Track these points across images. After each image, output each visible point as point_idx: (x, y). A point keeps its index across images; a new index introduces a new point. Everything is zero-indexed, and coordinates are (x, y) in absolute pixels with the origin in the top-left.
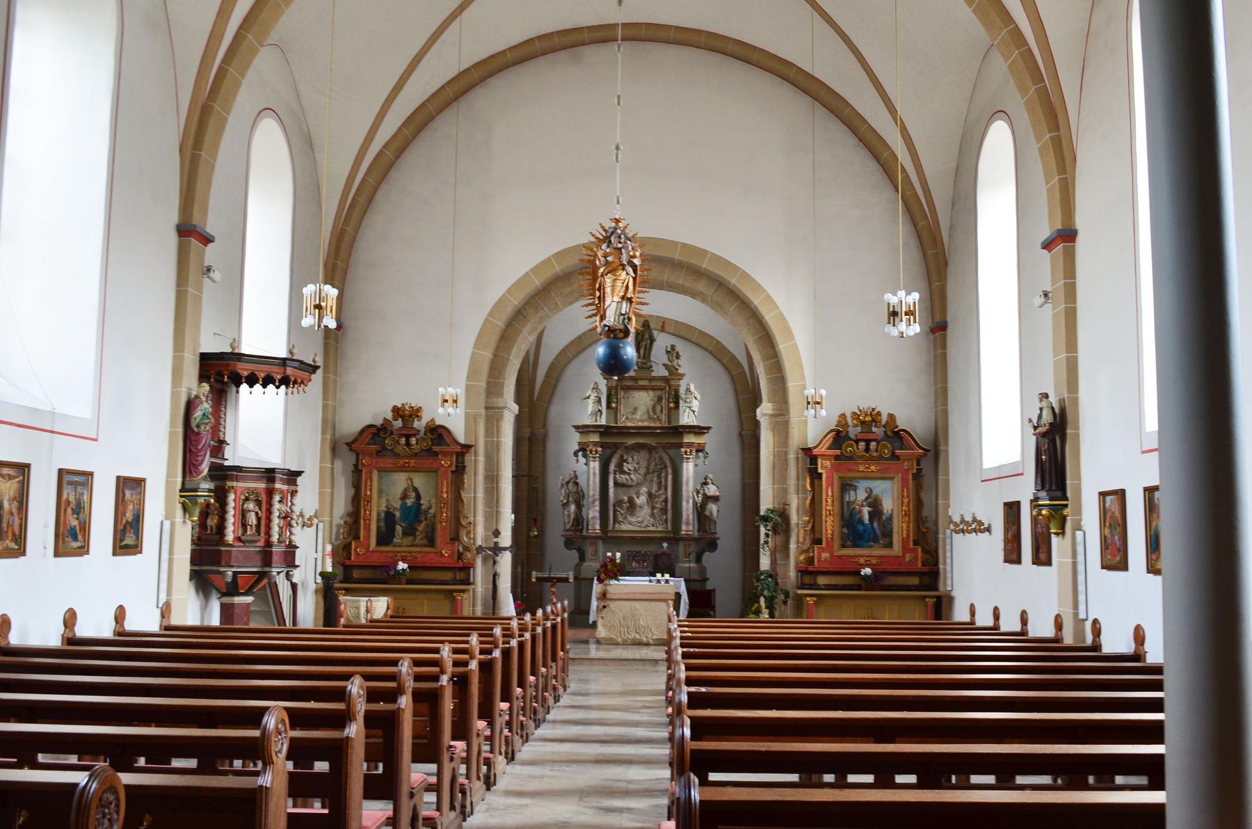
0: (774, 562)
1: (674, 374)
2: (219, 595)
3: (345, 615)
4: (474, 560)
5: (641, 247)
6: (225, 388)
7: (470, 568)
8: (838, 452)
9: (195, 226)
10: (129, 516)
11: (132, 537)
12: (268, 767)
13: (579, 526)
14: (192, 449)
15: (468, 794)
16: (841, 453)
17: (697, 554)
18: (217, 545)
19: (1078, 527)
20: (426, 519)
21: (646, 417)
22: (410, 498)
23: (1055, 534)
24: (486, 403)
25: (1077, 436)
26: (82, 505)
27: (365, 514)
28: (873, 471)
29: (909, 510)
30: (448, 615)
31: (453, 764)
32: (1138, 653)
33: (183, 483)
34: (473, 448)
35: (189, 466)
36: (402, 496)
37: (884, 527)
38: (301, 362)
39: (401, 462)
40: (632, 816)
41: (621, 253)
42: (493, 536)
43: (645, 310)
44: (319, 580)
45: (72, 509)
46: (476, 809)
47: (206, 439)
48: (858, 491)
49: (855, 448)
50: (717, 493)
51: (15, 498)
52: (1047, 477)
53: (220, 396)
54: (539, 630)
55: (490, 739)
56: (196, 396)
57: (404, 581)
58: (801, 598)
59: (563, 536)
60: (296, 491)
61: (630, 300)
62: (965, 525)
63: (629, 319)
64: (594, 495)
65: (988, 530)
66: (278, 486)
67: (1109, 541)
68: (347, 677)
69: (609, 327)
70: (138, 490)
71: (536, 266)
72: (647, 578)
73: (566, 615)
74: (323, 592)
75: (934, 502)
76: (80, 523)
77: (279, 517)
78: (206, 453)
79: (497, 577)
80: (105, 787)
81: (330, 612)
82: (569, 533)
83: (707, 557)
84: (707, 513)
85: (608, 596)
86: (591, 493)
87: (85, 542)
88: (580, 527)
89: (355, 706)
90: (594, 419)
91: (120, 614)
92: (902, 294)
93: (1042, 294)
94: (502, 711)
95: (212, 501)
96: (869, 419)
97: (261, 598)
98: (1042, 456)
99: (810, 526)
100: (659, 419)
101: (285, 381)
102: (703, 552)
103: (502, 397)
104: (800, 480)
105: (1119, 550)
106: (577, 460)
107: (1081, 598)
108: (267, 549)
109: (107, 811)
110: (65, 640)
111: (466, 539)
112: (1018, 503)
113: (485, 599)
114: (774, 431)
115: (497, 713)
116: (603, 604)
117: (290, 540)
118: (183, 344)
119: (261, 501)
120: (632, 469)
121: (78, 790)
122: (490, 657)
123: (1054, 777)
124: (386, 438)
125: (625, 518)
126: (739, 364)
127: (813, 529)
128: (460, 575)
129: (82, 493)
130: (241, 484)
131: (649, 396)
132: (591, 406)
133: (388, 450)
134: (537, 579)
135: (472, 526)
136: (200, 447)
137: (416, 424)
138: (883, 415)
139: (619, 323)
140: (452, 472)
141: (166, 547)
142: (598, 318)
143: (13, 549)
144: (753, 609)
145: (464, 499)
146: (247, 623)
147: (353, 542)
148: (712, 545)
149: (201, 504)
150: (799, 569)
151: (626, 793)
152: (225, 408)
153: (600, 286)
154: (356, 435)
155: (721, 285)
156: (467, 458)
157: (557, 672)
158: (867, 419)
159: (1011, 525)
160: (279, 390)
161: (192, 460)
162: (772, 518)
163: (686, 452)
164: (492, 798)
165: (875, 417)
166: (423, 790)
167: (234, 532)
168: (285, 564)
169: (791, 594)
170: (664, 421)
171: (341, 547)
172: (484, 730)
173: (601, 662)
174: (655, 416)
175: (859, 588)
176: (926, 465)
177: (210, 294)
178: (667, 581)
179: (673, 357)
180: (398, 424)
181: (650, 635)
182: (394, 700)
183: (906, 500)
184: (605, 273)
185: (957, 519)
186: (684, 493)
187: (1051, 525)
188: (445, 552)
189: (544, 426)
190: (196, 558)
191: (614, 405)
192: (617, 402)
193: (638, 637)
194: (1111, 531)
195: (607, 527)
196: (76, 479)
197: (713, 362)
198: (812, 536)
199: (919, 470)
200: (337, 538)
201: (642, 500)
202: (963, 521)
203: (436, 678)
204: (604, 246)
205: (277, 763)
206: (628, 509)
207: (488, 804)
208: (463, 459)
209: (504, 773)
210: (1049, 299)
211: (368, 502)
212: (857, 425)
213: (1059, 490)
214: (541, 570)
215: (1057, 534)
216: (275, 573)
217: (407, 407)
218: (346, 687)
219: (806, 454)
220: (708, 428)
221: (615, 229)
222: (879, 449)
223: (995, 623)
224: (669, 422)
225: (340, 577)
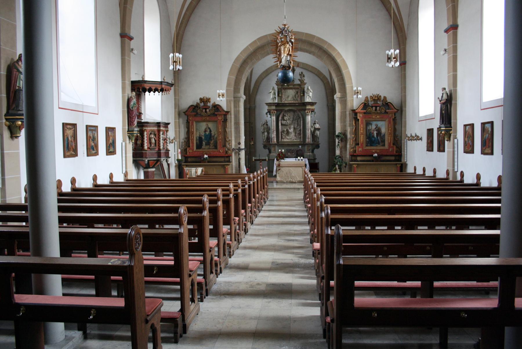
0: (341, 152)
1: (302, 83)
2: (143, 168)
4: (231, 154)
5: (294, 35)
6: (140, 93)
7: (230, 156)
8: (365, 111)
9: (127, 34)
10: (111, 141)
14: (131, 116)
16: (366, 111)
18: (141, 150)
19: (455, 138)
21: (292, 99)
23: (446, 140)
24: (234, 95)
25: (456, 104)
27: (191, 138)
28: (378, 118)
29: (391, 132)
30: (223, 173)
32: (478, 183)
34: (230, 113)
35: (130, 122)
37: (382, 138)
38: (167, 83)
39: (204, 118)
40: (298, 243)
41: (287, 37)
42: (238, 145)
43: (296, 59)
44: (176, 162)
46: (243, 241)
47: (135, 113)
48: (372, 125)
49: (371, 109)
50: (319, 127)
51: (72, 136)
52: (445, 119)
54: (259, 178)
55: (245, 216)
57: (207, 162)
58: (351, 165)
59: (263, 144)
60: (168, 130)
61: (290, 55)
62: (412, 137)
63: (291, 62)
64: (274, 129)
65: (421, 139)
66: (162, 128)
67: (467, 143)
68: (202, 195)
69: (283, 66)
70: (113, 132)
72: (295, 159)
73: (267, 172)
74: (178, 166)
75: (400, 129)
76: (95, 144)
77: (162, 140)
78: (136, 118)
79: (240, 159)
80: (136, 233)
81: (181, 173)
82: (265, 143)
83: (316, 151)
84: (316, 134)
85: (280, 165)
86: (273, 128)
88: (269, 141)
89: (206, 205)
90: (273, 101)
91: (111, 176)
92: (392, 51)
93: (444, 50)
94: (249, 206)
95: (139, 135)
96: (376, 99)
97: (157, 169)
98: (442, 111)
99: (355, 139)
100: (298, 101)
101: (162, 90)
102: (314, 149)
104: (351, 121)
105: (471, 146)
106: (267, 116)
107: (456, 164)
109: (137, 241)
110: (94, 185)
111: (228, 146)
112: (433, 129)
113: (236, 168)
114: (341, 104)
115: (247, 207)
116: (278, 168)
118: (125, 78)
122: (244, 188)
123: (446, 227)
124: (198, 110)
125: (285, 137)
126: (327, 79)
127: (356, 140)
128: (227, 159)
129: (95, 134)
131: (293, 91)
132: (272, 96)
134: (255, 160)
136: (133, 115)
137: (208, 104)
139: (286, 64)
140: (223, 121)
141: (124, 152)
142: (279, 62)
143: (73, 154)
144: (334, 169)
146: (153, 178)
147: (188, 148)
148: (318, 146)
149: (135, 136)
150: (350, 154)
151: (294, 235)
152: (141, 101)
153: (279, 50)
155: (320, 48)
156: (228, 116)
157: (265, 193)
158: (376, 98)
159: (429, 137)
161: (131, 120)
162: (340, 136)
163: (307, 112)
164: (247, 237)
166: (226, 234)
167: (147, 145)
168: (166, 156)
169: (348, 163)
170: (299, 101)
171: (184, 149)
173: (279, 189)
174: (296, 99)
175: (373, 161)
176: (398, 115)
177: (133, 58)
178: (302, 160)
179: (302, 76)
180: (202, 104)
181: (296, 179)
182: (216, 203)
183: (390, 129)
184: (281, 44)
185: (409, 135)
186: (307, 127)
187: (445, 137)
188: (221, 151)
189: (254, 104)
190: (135, 155)
191: (280, 95)
192: (281, 94)
193: (292, 180)
195: (279, 140)
197: (317, 78)
198: (355, 142)
201: (291, 130)
202: (411, 136)
204: (280, 35)
206: (286, 134)
208: (226, 116)
209: (250, 228)
210: (446, 52)
211: (192, 133)
212: (372, 101)
213: (449, 124)
214: (255, 157)
215: (447, 140)
216: (162, 160)
217: (205, 98)
218: (202, 199)
219: (353, 112)
220: (316, 103)
221: (284, 28)
222: (380, 110)
224: (301, 101)
225: (184, 161)
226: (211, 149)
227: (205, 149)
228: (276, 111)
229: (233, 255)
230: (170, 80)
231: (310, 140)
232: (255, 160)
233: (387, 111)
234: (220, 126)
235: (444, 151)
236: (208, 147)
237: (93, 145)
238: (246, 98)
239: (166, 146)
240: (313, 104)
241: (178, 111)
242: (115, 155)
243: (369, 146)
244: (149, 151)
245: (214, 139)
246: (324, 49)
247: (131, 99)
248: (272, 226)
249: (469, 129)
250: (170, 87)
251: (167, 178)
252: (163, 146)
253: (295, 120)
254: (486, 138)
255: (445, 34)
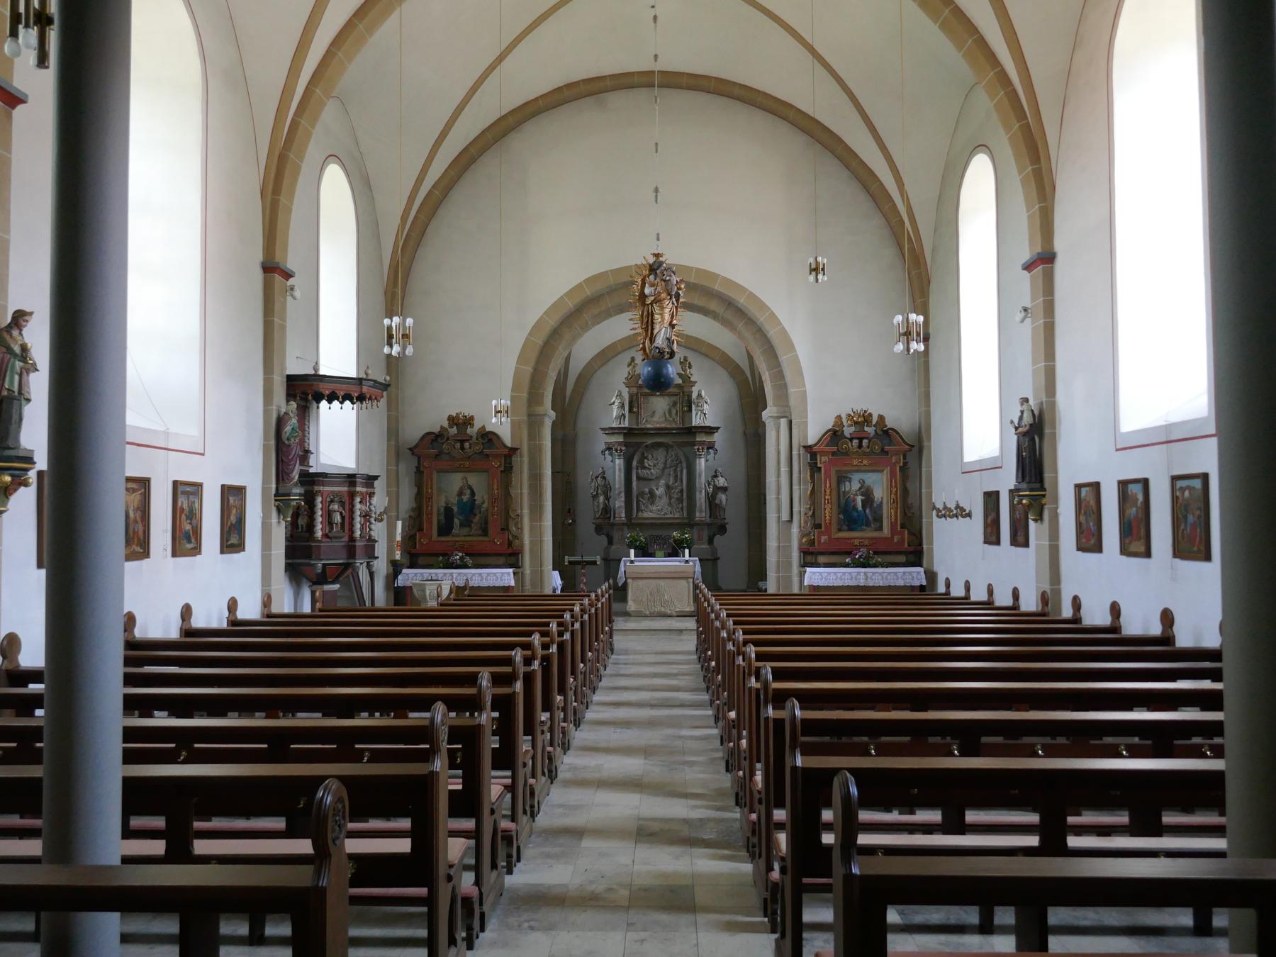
1: (686, 379)
6: (308, 405)
7: (518, 554)
9: (278, 263)
10: (233, 519)
11: (236, 537)
13: (607, 514)
14: (284, 458)
17: (709, 537)
18: (307, 541)
21: (663, 419)
23: (1033, 520)
25: (1054, 435)
26: (194, 511)
29: (897, 498)
33: (277, 489)
34: (519, 451)
35: (282, 475)
38: (375, 381)
39: (457, 464)
45: (186, 515)
47: (296, 451)
49: (850, 445)
51: (138, 508)
53: (304, 412)
55: (564, 709)
56: (285, 413)
59: (593, 523)
60: (374, 493)
64: (619, 488)
65: (969, 515)
66: (359, 489)
67: (1084, 526)
70: (240, 497)
71: (570, 291)
73: (611, 591)
76: (192, 527)
77: (360, 516)
82: (600, 521)
83: (718, 539)
86: (617, 486)
87: (197, 543)
88: (609, 515)
93: (1021, 309)
95: (303, 503)
97: (346, 585)
98: (1022, 453)
100: (676, 423)
101: (361, 398)
108: (350, 544)
112: (998, 493)
117: (370, 535)
119: (344, 503)
120: (652, 464)
121: (316, 800)
125: (647, 507)
126: (743, 372)
129: (194, 502)
130: (326, 488)
132: (615, 412)
134: (569, 562)
136: (290, 457)
137: (469, 430)
138: (873, 416)
140: (501, 471)
145: (513, 495)
148: (722, 529)
149: (294, 506)
152: (309, 422)
154: (417, 442)
163: (698, 449)
165: (866, 418)
167: (322, 529)
174: (671, 419)
180: (454, 430)
183: (894, 490)
185: (940, 506)
186: (697, 485)
190: (291, 552)
194: (1086, 519)
195: (632, 515)
196: (188, 489)
199: (905, 464)
201: (660, 491)
202: (945, 508)
206: (649, 499)
210: (1028, 313)
211: (429, 499)
220: (719, 428)
223: (989, 598)
227: (458, 536)
228: (625, 446)
230: (382, 377)
231: (704, 514)
233: (887, 448)
234: (495, 481)
235: (1026, 544)
236: (466, 530)
237: (189, 530)
238: (556, 416)
239: (368, 530)
240: (712, 431)
242: (242, 553)
243: (844, 530)
244: (328, 542)
245: (480, 513)
246: (739, 306)
247: (286, 417)
249: (1088, 496)
251: (368, 604)
253: (670, 468)
254: (1132, 516)
255: (1026, 272)
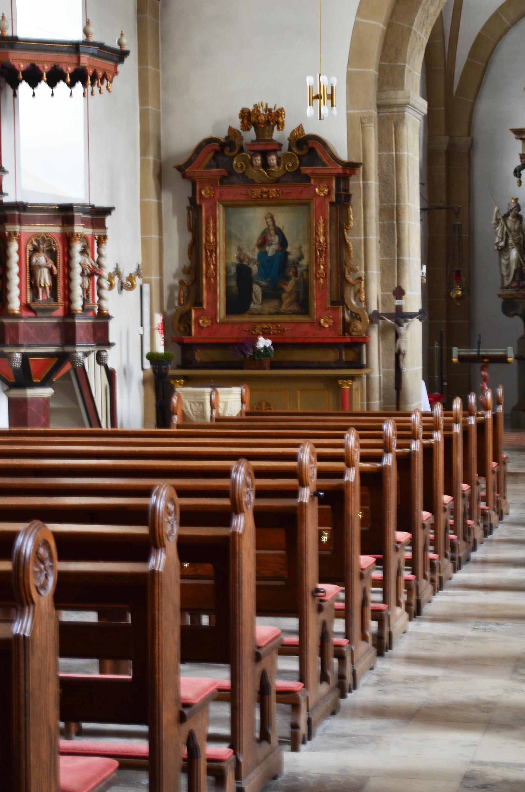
2: (6, 387)
3: (179, 412)
4: (367, 333)
12: (27, 610)
15: (348, 659)
20: (296, 275)
22: (272, 244)
24: (378, 99)
30: (332, 411)
31: (322, 616)
36: (260, 241)
38: (101, 46)
39: (257, 192)
42: (393, 297)
44: (147, 365)
46: (362, 681)
54: (457, 429)
57: (267, 364)
59: (499, 296)
60: (105, 237)
73: (500, 409)
77: (82, 274)
79: (401, 357)
82: (510, 291)
89: (161, 526)
94: (399, 542)
103: (403, 89)
111: (354, 302)
113: (384, 390)
122: (379, 465)
124: (233, 158)
128: (346, 356)
133: (237, 175)
135: (363, 282)
137: (276, 135)
140: (331, 204)
146: (46, 424)
147: (193, 311)
156: (352, 182)
160: (74, 90)
166: (275, 652)
167: (20, 297)
172: (370, 569)
180: (251, 135)
182: (227, 523)
188: (325, 322)
189: (469, 133)
200: (170, 304)
203: (294, 494)
205: (39, 602)
207: (378, 675)
209: (404, 632)
214: (469, 345)
216: (80, 355)
217: (262, 111)
226: (283, 314)
229: (309, 738)
232: (461, 358)
234: (321, 221)
236: (271, 305)
241: (155, 162)
244: (29, 318)
245: (296, 275)
248: (496, 627)
250: (112, 63)
251: (105, 425)
252: (85, 301)
